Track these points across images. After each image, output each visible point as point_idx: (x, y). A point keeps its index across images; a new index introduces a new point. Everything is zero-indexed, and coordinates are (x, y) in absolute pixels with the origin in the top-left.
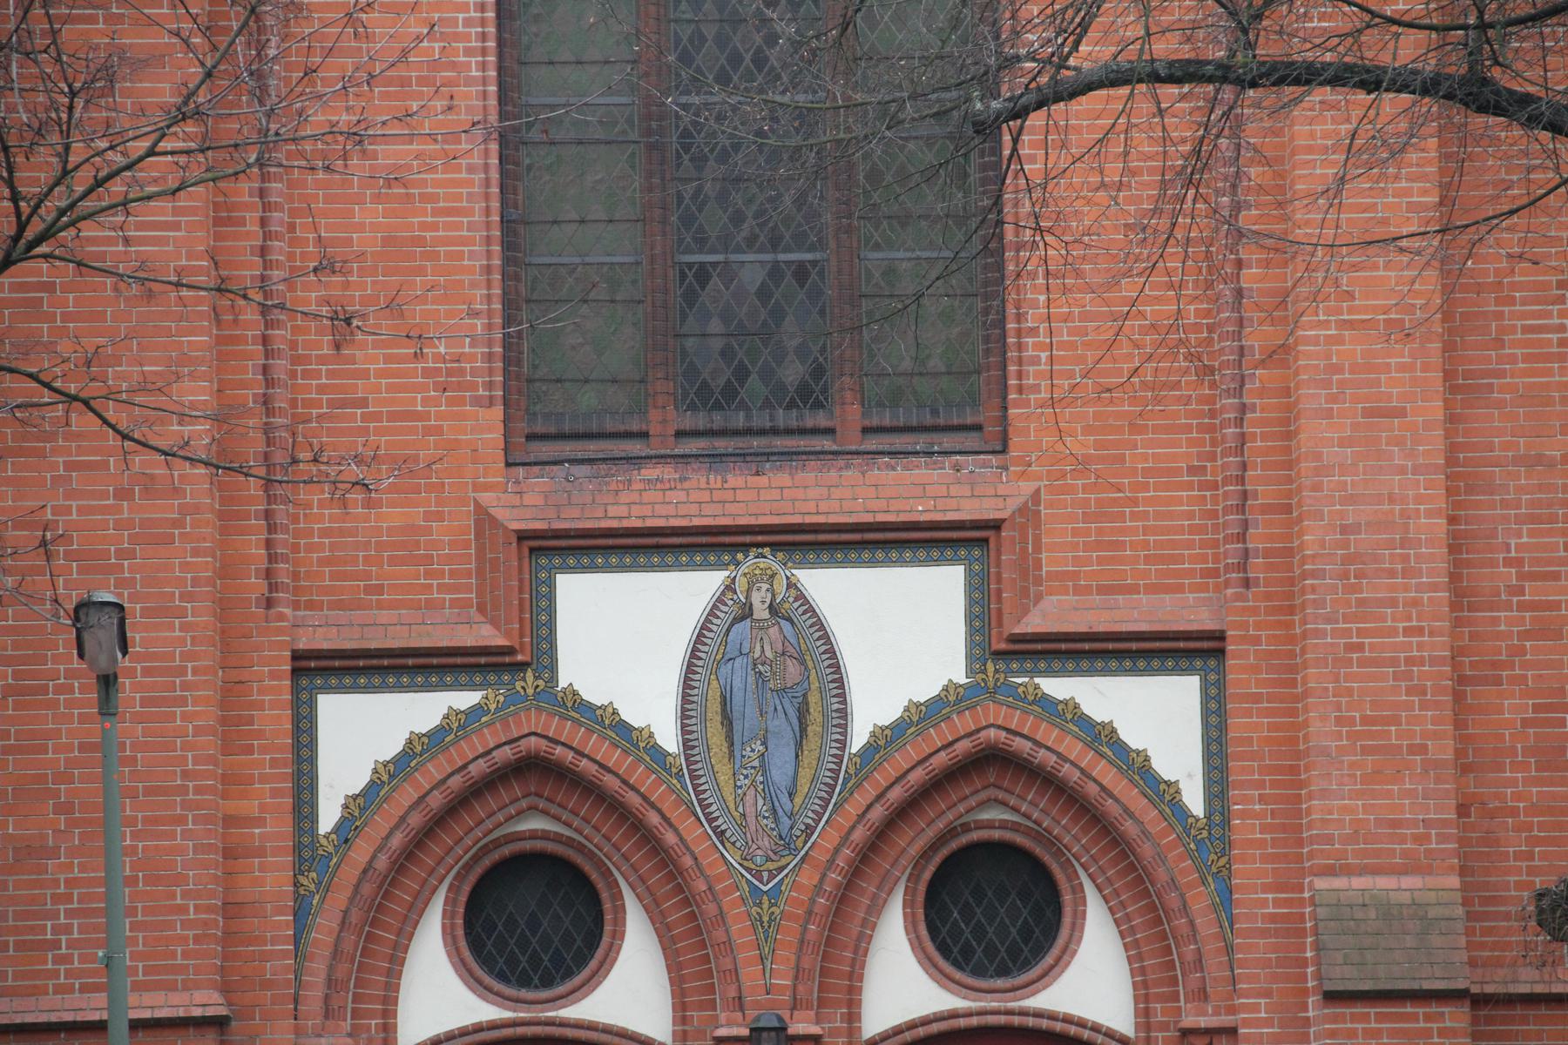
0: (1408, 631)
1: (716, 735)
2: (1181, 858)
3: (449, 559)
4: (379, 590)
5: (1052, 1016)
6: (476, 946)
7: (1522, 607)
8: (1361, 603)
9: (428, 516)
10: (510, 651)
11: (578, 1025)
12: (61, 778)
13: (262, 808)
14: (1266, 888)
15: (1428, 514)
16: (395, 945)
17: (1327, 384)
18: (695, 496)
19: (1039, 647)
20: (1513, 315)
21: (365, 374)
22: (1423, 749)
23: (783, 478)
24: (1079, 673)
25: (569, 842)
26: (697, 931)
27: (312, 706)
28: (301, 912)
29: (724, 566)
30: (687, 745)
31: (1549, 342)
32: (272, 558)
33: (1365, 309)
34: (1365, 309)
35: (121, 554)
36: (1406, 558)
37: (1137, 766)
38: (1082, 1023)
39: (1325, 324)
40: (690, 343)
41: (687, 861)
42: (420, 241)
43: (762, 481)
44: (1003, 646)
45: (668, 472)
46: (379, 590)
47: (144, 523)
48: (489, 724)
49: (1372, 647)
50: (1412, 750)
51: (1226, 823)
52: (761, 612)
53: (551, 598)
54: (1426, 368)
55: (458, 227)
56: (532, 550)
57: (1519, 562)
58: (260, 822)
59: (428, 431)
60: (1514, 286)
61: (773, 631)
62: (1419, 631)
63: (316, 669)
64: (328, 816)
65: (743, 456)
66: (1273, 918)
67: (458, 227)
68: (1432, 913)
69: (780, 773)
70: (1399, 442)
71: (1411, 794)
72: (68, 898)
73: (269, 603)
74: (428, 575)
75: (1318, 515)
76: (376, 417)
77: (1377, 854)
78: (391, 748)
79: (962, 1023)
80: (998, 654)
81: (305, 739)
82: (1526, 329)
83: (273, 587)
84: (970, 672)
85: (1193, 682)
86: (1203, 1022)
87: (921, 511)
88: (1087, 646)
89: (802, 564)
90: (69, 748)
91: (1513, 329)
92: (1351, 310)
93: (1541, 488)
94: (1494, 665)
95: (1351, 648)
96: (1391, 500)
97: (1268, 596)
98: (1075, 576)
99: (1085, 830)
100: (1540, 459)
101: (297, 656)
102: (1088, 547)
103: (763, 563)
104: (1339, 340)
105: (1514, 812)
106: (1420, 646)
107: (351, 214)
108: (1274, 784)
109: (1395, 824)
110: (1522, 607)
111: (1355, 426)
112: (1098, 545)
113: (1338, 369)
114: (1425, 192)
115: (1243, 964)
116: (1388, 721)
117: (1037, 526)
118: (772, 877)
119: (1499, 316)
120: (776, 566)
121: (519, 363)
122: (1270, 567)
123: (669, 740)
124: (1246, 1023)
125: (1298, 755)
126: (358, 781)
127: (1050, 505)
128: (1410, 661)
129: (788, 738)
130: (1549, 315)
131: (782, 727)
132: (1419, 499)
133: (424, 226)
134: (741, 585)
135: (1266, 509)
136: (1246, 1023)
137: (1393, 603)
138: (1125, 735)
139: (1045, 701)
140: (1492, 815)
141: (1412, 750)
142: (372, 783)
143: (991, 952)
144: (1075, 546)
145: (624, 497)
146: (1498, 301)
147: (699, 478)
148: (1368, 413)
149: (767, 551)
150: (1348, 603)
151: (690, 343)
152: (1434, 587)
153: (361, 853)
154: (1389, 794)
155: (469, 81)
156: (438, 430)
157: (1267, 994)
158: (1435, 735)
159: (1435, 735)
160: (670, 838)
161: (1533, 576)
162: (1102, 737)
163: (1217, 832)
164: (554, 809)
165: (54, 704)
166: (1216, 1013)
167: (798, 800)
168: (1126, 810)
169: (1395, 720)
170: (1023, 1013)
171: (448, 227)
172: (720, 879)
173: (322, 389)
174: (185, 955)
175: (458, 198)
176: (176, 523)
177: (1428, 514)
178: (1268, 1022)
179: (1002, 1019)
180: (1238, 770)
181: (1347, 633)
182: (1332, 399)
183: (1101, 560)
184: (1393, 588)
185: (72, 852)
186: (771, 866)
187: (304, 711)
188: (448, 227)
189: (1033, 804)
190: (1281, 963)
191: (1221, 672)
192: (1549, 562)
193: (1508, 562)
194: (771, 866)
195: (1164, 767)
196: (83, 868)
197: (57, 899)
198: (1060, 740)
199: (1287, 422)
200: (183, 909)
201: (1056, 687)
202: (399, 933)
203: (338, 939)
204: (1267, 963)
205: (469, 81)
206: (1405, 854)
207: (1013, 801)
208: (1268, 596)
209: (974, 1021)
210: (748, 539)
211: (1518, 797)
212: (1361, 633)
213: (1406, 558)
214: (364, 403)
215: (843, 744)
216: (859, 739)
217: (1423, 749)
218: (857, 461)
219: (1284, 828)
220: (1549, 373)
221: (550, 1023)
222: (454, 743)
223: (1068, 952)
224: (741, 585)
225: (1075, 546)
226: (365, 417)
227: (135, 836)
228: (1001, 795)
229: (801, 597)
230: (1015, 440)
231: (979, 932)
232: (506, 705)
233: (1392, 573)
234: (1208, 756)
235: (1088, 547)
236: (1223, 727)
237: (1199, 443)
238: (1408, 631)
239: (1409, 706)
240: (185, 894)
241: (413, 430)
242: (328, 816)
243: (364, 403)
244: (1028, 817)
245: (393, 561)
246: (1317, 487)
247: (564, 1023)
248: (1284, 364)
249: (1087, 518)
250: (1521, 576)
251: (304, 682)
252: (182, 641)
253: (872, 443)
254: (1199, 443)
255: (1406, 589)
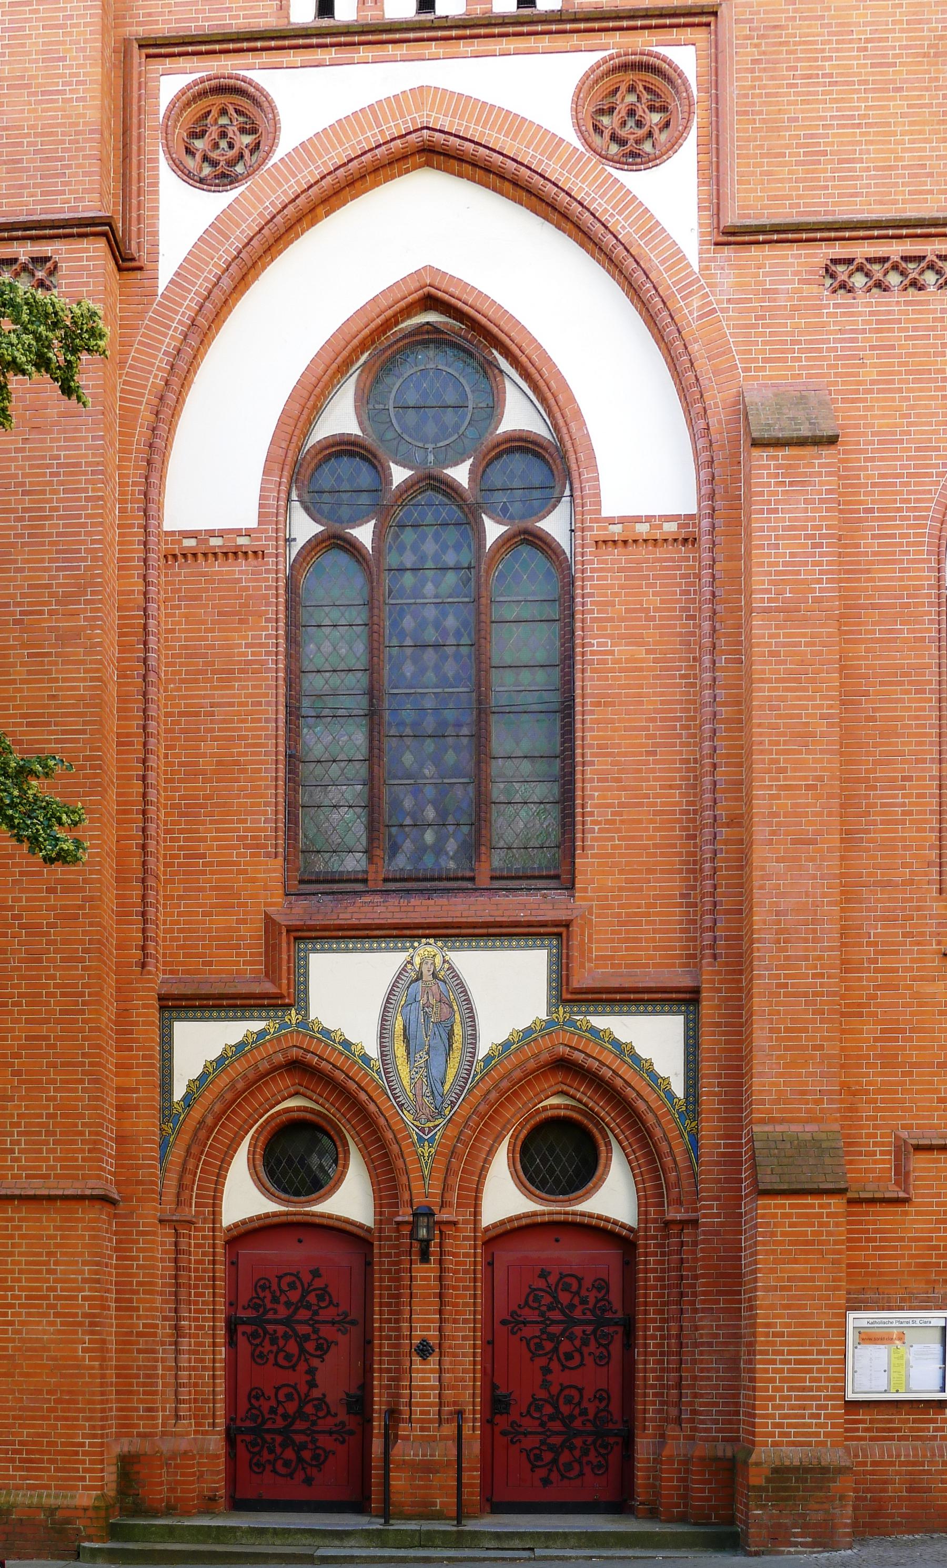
0: (815, 976)
1: (400, 1050)
2: (669, 1122)
3: (249, 946)
4: (210, 964)
5: (591, 1216)
6: (271, 1173)
7: (877, 970)
8: (787, 958)
9: (239, 921)
10: (281, 997)
11: (322, 1215)
12: (17, 1056)
13: (137, 1082)
14: (720, 1137)
15: (830, 904)
16: (220, 1168)
17: (770, 824)
18: (391, 909)
19: (590, 996)
20: (875, 797)
21: (204, 839)
22: (821, 1047)
23: (444, 901)
24: (612, 1013)
25: (319, 1113)
26: (389, 1163)
27: (171, 1028)
28: (164, 1145)
29: (404, 949)
30: (383, 1054)
31: (896, 813)
32: (145, 939)
33: (794, 778)
34: (794, 778)
35: (49, 925)
36: (814, 931)
37: (644, 1067)
38: (607, 1220)
39: (770, 787)
40: (394, 830)
41: (382, 1121)
42: (237, 763)
43: (431, 902)
44: (569, 996)
45: (377, 899)
46: (210, 964)
47: (63, 907)
48: (270, 1041)
49: (793, 985)
50: (815, 1048)
51: (696, 1102)
52: (427, 976)
53: (306, 967)
54: (830, 814)
55: (258, 754)
56: (296, 939)
57: (875, 944)
58: (136, 1090)
59: (240, 872)
60: (876, 779)
61: (434, 988)
62: (822, 975)
63: (173, 1007)
64: (179, 1092)
65: (421, 891)
66: (723, 1155)
67: (258, 754)
68: (824, 1145)
69: (436, 1073)
70: (812, 859)
71: (813, 1074)
72: (18, 1125)
73: (144, 965)
74: (238, 955)
75: (762, 904)
76: (210, 864)
77: (791, 1111)
78: (215, 1054)
79: (539, 1219)
80: (565, 1002)
81: (166, 1047)
82: (883, 805)
83: (146, 956)
84: (549, 1013)
85: (680, 1019)
86: (679, 1217)
87: (522, 916)
88: (618, 996)
89: (451, 949)
90: (20, 1038)
91: (875, 805)
92: (785, 779)
93: (890, 900)
94: (859, 1005)
95: (779, 986)
96: (807, 895)
97: (727, 964)
98: (612, 958)
99: (613, 1108)
100: (889, 883)
101: (161, 998)
102: (620, 941)
103: (429, 948)
104: (778, 797)
105: (867, 1092)
106: (822, 985)
107: (199, 748)
108: (727, 1076)
109: (803, 1093)
110: (877, 970)
111: (786, 850)
112: (627, 940)
113: (776, 815)
114: (830, 707)
115: (702, 1181)
116: (800, 1030)
117: (591, 928)
118: (430, 1131)
119: (867, 797)
120: (436, 950)
121: (296, 840)
122: (728, 947)
123: (373, 1051)
124: (705, 1216)
125: (741, 1059)
126: (196, 1071)
127: (598, 916)
128: (815, 994)
129: (442, 1050)
130: (896, 796)
131: (439, 1044)
132: (824, 895)
133: (240, 754)
134: (417, 960)
135: (727, 912)
136: (705, 1216)
137: (806, 958)
138: (638, 1050)
139: (593, 1031)
140: (854, 1094)
141: (815, 1048)
142: (203, 1074)
143: (557, 1182)
144: (613, 941)
145: (351, 909)
146: (867, 788)
147: (393, 901)
148: (794, 842)
149: (432, 941)
150: (779, 958)
151: (394, 830)
152: (831, 949)
153: (197, 1113)
154: (799, 1075)
155: (268, 670)
156: (245, 872)
157: (717, 1198)
158: (829, 1039)
159: (829, 1039)
160: (372, 1107)
161: (883, 953)
162: (624, 1051)
163: (691, 1107)
164: (309, 1093)
165: (11, 1013)
166: (687, 1211)
167: (447, 1087)
168: (638, 1094)
169: (806, 1030)
170: (574, 1213)
171: (253, 753)
172: (400, 1131)
173: (180, 848)
174: (84, 1159)
175: (259, 737)
176: (81, 907)
177: (830, 904)
178: (718, 1215)
179: (562, 1217)
180: (706, 1068)
181: (778, 977)
182: (773, 833)
183: (627, 949)
184: (806, 949)
185: (21, 1099)
186: (431, 1124)
187: (166, 1031)
188: (253, 753)
189: (584, 1093)
190: (727, 1180)
191: (697, 1013)
192: (893, 943)
193: (869, 944)
194: (431, 1124)
195: (661, 1069)
196: (27, 1107)
197: (13, 1125)
198: (600, 1053)
199: (741, 859)
200: (82, 1133)
201: (599, 1022)
202: (223, 1161)
203: (185, 1162)
204: (718, 1181)
205: (268, 670)
206: (808, 1111)
207: (572, 1091)
208: (727, 964)
209: (546, 1218)
210: (420, 932)
211: (869, 1083)
212: (786, 976)
213: (814, 931)
214: (203, 856)
215: (474, 1054)
216: (482, 1052)
217: (821, 1047)
218: (486, 893)
219: (732, 1102)
220: (896, 831)
221: (307, 1214)
222: (250, 1051)
223: (602, 1180)
224: (417, 960)
225: (613, 941)
226: (204, 864)
227: (56, 1090)
228: (565, 1088)
229: (451, 968)
230: (579, 878)
231: (551, 1171)
232: (280, 1029)
233: (806, 940)
234: (687, 1062)
235: (620, 941)
236: (697, 1045)
237: (688, 879)
238: (815, 976)
239: (814, 1021)
240: (84, 1125)
241: (231, 872)
242: (179, 1092)
243: (203, 856)
244: (580, 1101)
245: (218, 947)
246: (762, 887)
247: (314, 1214)
248: (740, 825)
249: (620, 924)
250: (876, 953)
251: (166, 1014)
252: (83, 977)
253: (497, 884)
254: (688, 879)
255: (815, 949)
